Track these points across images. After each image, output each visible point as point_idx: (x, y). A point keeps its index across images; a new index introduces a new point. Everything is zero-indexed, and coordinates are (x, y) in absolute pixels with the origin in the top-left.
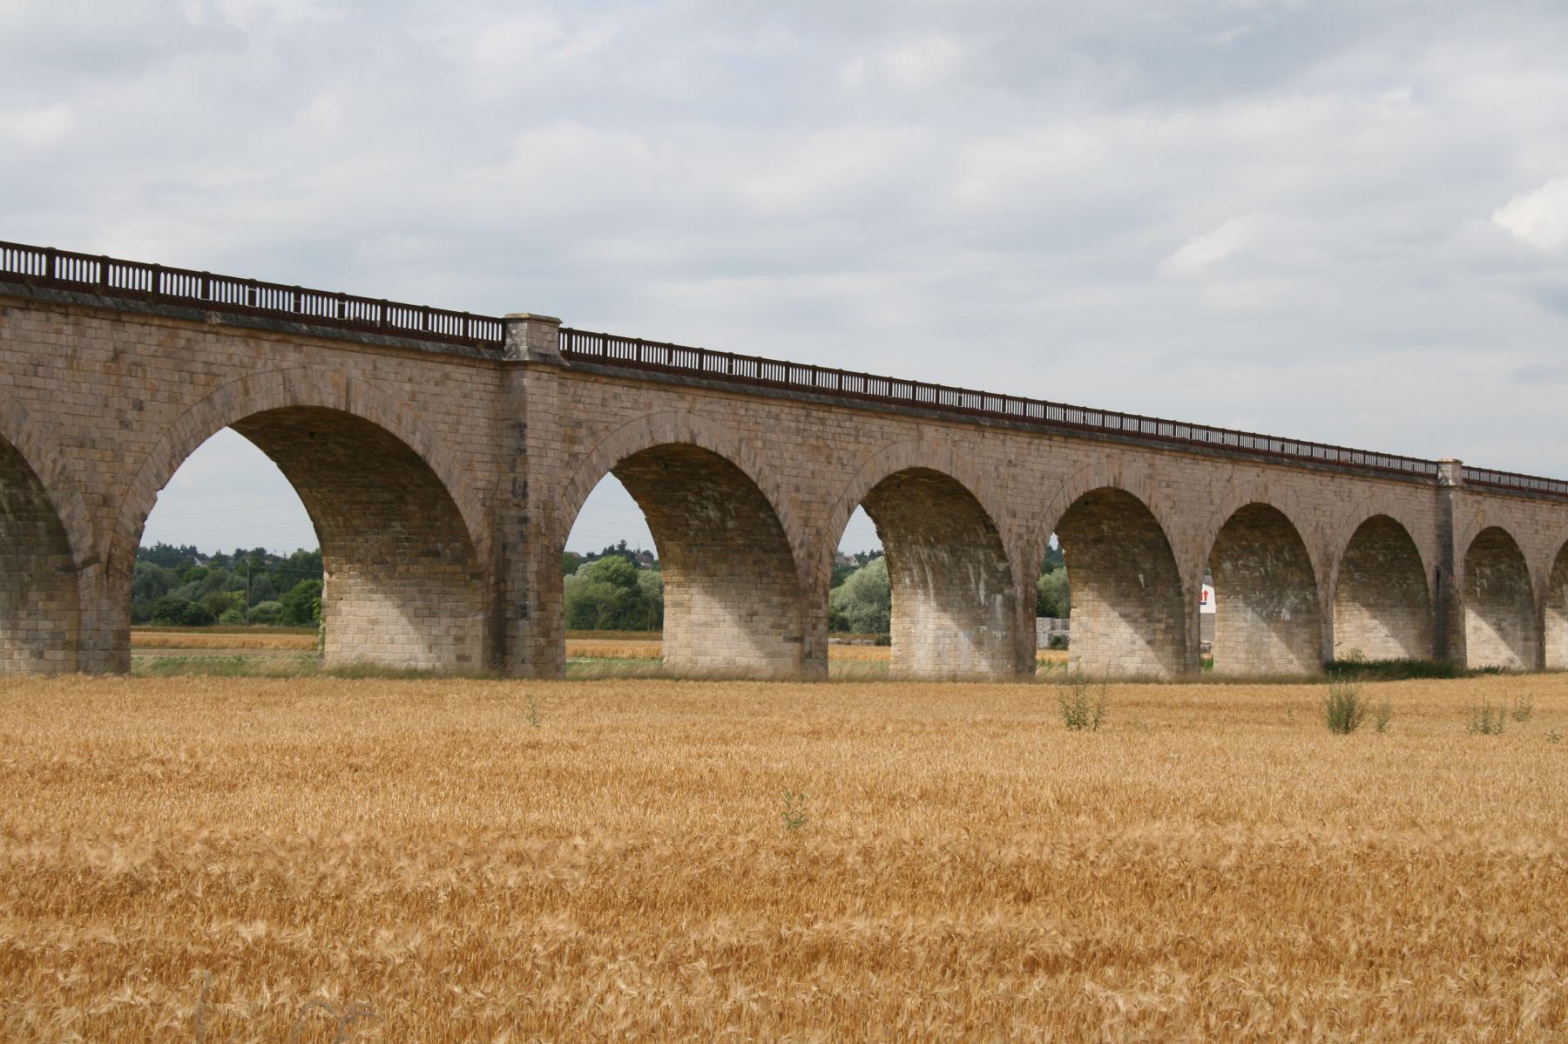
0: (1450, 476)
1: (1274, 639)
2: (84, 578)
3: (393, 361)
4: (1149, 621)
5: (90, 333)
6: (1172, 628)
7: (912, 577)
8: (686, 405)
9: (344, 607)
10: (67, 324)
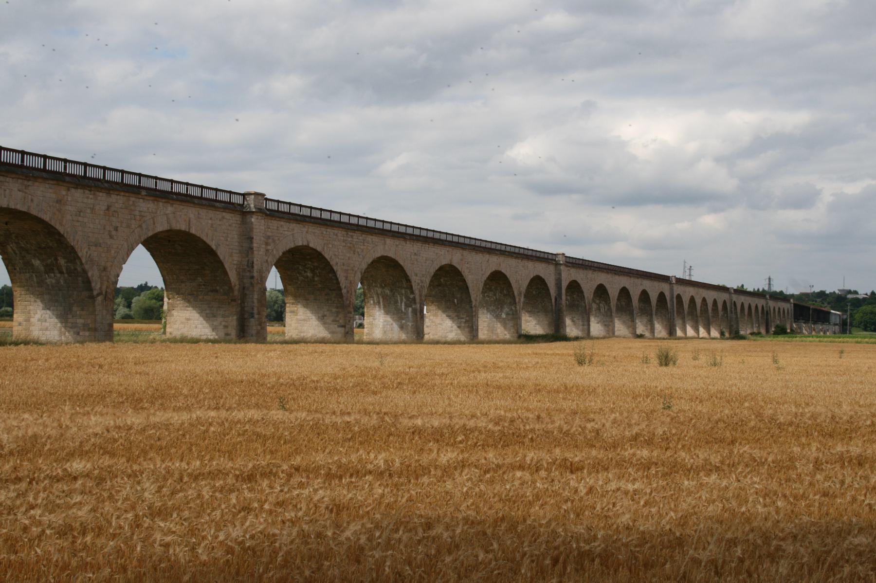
0: (561, 260)
1: (499, 325)
2: (97, 301)
3: (205, 211)
4: (459, 318)
5: (99, 198)
6: (468, 321)
7: (373, 300)
8: (306, 230)
9: (175, 313)
10: (91, 194)
